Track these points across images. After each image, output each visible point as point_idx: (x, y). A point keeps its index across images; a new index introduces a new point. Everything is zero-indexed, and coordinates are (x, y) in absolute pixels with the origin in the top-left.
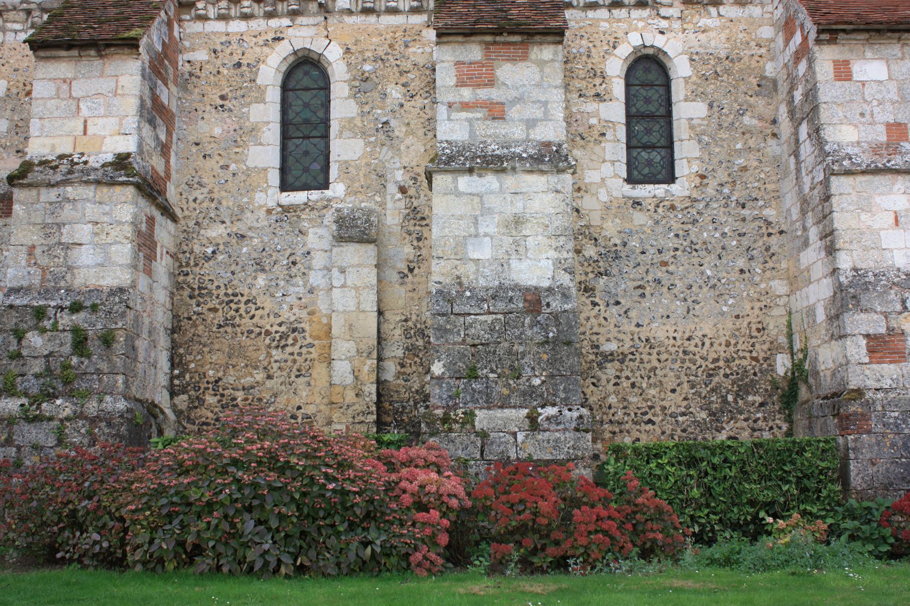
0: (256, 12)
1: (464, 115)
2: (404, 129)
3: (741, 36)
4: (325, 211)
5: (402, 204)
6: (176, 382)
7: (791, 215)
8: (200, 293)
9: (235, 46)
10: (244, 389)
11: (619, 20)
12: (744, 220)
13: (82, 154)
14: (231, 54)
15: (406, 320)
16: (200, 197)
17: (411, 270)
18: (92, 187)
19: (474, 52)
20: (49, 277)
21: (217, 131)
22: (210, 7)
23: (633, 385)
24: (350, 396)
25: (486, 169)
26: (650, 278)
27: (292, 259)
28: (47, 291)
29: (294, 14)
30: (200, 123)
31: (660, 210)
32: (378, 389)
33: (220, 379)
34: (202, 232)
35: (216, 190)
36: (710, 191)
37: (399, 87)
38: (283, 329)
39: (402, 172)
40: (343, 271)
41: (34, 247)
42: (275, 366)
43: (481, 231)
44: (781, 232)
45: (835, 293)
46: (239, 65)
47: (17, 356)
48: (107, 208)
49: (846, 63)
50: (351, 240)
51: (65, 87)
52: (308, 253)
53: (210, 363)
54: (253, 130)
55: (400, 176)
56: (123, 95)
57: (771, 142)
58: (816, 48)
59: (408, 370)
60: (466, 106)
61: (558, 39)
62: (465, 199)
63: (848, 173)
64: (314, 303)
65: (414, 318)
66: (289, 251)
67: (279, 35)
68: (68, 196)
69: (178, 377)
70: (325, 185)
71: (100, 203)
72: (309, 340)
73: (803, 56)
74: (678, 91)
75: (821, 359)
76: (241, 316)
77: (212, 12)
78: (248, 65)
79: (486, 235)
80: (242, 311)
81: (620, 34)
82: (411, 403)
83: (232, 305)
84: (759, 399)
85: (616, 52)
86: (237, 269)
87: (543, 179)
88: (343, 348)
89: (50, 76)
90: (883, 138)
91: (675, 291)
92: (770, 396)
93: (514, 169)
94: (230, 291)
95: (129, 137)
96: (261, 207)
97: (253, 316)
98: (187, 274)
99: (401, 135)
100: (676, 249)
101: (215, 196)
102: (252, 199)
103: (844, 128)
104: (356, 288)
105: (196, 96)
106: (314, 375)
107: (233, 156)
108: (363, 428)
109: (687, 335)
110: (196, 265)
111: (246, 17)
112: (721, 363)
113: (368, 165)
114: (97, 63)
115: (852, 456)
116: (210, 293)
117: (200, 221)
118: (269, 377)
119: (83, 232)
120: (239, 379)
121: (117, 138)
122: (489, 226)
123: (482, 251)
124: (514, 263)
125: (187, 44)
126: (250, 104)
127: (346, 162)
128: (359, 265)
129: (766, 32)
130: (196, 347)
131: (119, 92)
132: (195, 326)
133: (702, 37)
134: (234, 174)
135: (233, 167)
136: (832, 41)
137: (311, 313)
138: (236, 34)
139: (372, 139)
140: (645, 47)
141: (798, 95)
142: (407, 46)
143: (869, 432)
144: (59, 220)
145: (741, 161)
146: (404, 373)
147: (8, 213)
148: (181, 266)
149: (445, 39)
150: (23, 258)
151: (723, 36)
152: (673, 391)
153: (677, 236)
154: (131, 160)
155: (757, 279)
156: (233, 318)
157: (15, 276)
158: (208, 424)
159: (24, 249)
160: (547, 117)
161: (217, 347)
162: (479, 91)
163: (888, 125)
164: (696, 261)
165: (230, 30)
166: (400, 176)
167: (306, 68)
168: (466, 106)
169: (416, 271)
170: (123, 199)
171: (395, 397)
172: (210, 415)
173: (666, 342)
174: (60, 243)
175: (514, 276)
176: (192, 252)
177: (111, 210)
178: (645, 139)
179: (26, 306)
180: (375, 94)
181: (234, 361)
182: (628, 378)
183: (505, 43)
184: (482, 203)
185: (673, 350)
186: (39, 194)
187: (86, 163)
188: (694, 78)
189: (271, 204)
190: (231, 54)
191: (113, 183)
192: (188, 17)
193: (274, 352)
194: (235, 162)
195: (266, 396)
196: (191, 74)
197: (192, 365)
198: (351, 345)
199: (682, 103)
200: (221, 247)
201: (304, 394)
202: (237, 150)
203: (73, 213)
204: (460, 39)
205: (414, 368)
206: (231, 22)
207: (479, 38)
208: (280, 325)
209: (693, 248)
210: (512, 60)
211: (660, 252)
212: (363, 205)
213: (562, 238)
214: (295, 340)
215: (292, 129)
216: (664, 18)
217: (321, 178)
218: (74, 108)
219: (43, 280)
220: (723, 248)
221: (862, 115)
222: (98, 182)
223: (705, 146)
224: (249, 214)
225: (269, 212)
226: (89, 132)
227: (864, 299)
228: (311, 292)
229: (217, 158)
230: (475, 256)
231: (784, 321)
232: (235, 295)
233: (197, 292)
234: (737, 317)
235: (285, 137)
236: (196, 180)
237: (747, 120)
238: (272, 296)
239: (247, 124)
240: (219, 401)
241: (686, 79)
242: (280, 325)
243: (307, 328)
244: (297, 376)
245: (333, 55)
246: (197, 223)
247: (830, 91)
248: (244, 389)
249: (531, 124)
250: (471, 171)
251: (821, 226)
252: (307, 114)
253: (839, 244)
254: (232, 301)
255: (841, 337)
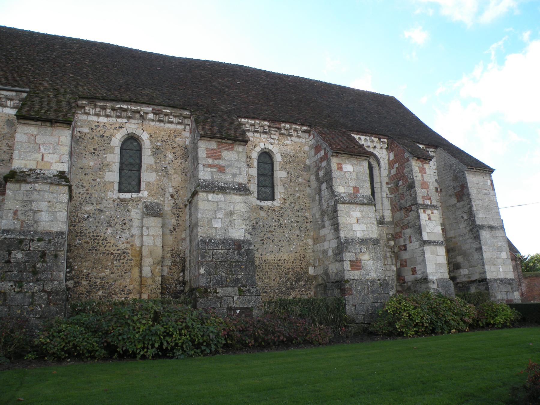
0: (112, 115)
1: (209, 169)
2: (173, 171)
3: (298, 149)
4: (138, 202)
5: (172, 202)
6: (68, 275)
7: (315, 216)
8: (81, 234)
9: (101, 128)
10: (100, 278)
11: (257, 138)
12: (298, 216)
13: (41, 170)
14: (100, 131)
15: (172, 250)
16: (82, 192)
17: (175, 229)
18: (48, 186)
19: (213, 145)
20: (25, 225)
21: (92, 164)
22: (91, 110)
23: (260, 278)
24: (150, 282)
25: (220, 192)
26: (266, 237)
27: (124, 222)
28: (24, 232)
29: (129, 118)
30: (84, 159)
31: (270, 211)
32: (162, 279)
33: (89, 274)
34: (82, 207)
35: (90, 189)
36: (287, 205)
37: (172, 154)
38: (119, 252)
39: (172, 188)
40: (148, 228)
41: (17, 211)
42: (115, 268)
43: (218, 216)
44: (311, 222)
45: (338, 245)
46: (103, 136)
47: (8, 262)
48: (55, 196)
49: (341, 164)
50: (152, 215)
51: (32, 138)
52: (131, 220)
53: (84, 266)
54: (108, 165)
55: (171, 190)
56: (62, 145)
57: (308, 188)
58: (331, 158)
59: (173, 271)
60: (210, 166)
61: (245, 144)
62: (211, 203)
63: (343, 203)
64: (133, 241)
65: (176, 249)
66: (122, 219)
67: (121, 126)
68: (36, 188)
69: (69, 272)
70: (139, 191)
71: (52, 193)
72: (131, 257)
73: (324, 160)
74: (277, 167)
75: (330, 268)
76: (100, 245)
77: (92, 112)
78: (107, 137)
79: (219, 218)
80: (100, 244)
81: (257, 143)
82: (174, 285)
83: (96, 241)
84: (303, 283)
85: (279, 154)
86: (99, 225)
87: (240, 197)
88: (147, 262)
89: (25, 133)
90: (352, 192)
91: (275, 242)
92: (307, 282)
93: (230, 193)
94: (95, 235)
95: (64, 164)
96: (110, 198)
97: (106, 246)
98: (75, 226)
99: (172, 173)
100: (275, 226)
101: (89, 192)
102: (106, 195)
103: (340, 187)
104: (153, 236)
105: (82, 147)
106: (133, 272)
107: (98, 175)
108: (155, 295)
109: (279, 259)
110: (79, 222)
111: (107, 116)
112: (290, 270)
113: (158, 184)
114: (50, 129)
115: (347, 303)
116: (85, 235)
117: (82, 202)
118: (112, 273)
119: (43, 205)
120: (98, 273)
121: (58, 164)
122: (220, 215)
123: (218, 224)
124: (230, 230)
125: (79, 124)
126: (107, 153)
127: (148, 182)
128: (155, 226)
129: (307, 148)
130: (78, 259)
131: (60, 143)
132: (78, 249)
133: (285, 147)
134: (99, 183)
135: (98, 180)
136: (336, 156)
137: (132, 246)
138: (102, 122)
139: (160, 174)
140: (265, 148)
141: (321, 173)
142: (175, 137)
143: (352, 295)
144: (31, 199)
145: (298, 195)
146: (171, 272)
147: (3, 193)
148: (72, 222)
149: (203, 138)
150: (11, 215)
151: (292, 148)
152: (274, 280)
153: (276, 221)
154: (65, 175)
155: (303, 238)
156: (96, 247)
157: (6, 224)
158: (83, 294)
159: (12, 211)
160: (240, 174)
161: (88, 259)
162: (215, 161)
163: (354, 187)
164: (282, 231)
165: (99, 120)
166: (171, 190)
167: (132, 141)
168: (210, 166)
169: (177, 230)
170: (63, 192)
171: (167, 282)
172: (84, 290)
173: (272, 261)
174: (31, 210)
175: (230, 235)
176: (77, 216)
177: (57, 196)
178: (264, 183)
179: (13, 238)
180: (162, 156)
181: (96, 266)
182: (258, 275)
183: (226, 143)
184: (218, 205)
185: (274, 264)
186: (20, 187)
187: (44, 174)
188: (282, 162)
189: (115, 197)
190: (100, 131)
191: (59, 185)
192: (80, 112)
193: (115, 262)
194: (100, 178)
195: (111, 281)
196: (80, 137)
197: (76, 267)
198: (151, 260)
199: (278, 171)
200: (91, 215)
201: (128, 281)
202: (100, 173)
203: (38, 196)
204: (209, 139)
205: (175, 270)
206: (100, 118)
207: (216, 140)
208: (118, 250)
209: (281, 226)
210: (228, 150)
211: (269, 227)
212: (155, 201)
213: (248, 221)
214: (125, 257)
215: (124, 166)
216: (273, 139)
217: (136, 188)
218: (37, 148)
219: (22, 226)
220: (291, 226)
221: (346, 183)
222: (52, 184)
223: (286, 189)
224: (105, 201)
225: (114, 201)
226: (45, 159)
227: (349, 247)
228: (132, 236)
229: (91, 175)
230: (216, 226)
231: (312, 254)
232: (97, 236)
233: (79, 234)
234: (296, 252)
235: (121, 169)
236: (81, 184)
237: (300, 180)
238: (114, 237)
239: (105, 162)
240: (88, 284)
241: (280, 162)
242: (118, 250)
243: (130, 252)
244: (125, 273)
245: (145, 136)
246: (80, 204)
247: (336, 174)
248: (100, 278)
249: (234, 175)
250: (213, 192)
251: (332, 221)
252: (131, 160)
253: (340, 228)
254: (96, 239)
255: (341, 261)
